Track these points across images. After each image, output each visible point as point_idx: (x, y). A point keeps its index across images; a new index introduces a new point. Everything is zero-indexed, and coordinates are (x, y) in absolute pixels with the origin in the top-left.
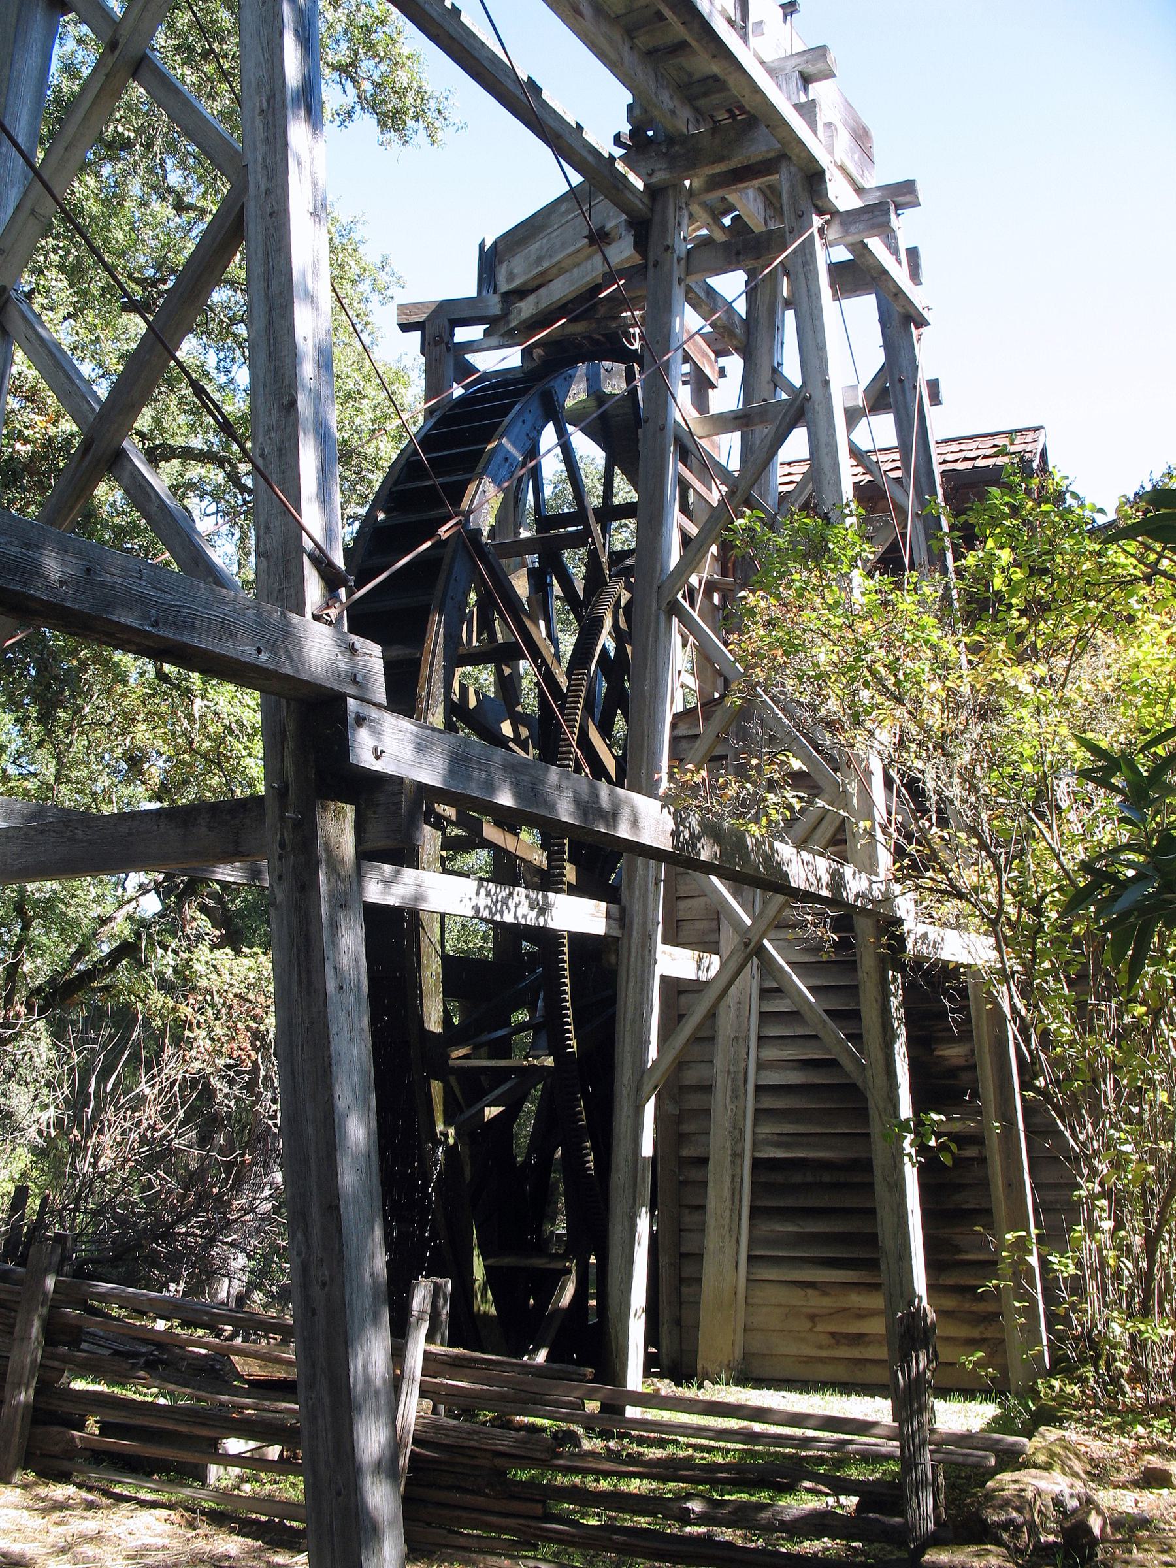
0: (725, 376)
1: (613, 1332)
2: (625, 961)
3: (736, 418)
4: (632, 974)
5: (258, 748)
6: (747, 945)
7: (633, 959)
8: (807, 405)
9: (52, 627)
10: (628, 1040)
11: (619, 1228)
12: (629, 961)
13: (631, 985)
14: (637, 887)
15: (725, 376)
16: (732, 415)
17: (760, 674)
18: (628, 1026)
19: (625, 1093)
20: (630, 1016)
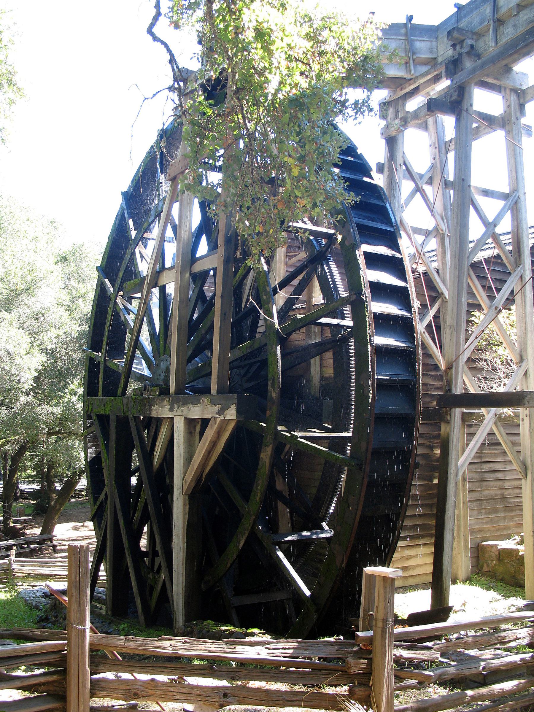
0: (300, 75)
1: (444, 580)
2: (453, 419)
3: (483, 191)
4: (456, 425)
5: (318, 340)
6: (496, 416)
7: (456, 418)
8: (519, 200)
9: (14, 476)
10: (454, 453)
11: (448, 535)
12: (455, 418)
13: (455, 430)
14: (458, 387)
15: (300, 75)
16: (481, 189)
17: (351, 64)
18: (454, 448)
19: (452, 477)
20: (454, 443)
